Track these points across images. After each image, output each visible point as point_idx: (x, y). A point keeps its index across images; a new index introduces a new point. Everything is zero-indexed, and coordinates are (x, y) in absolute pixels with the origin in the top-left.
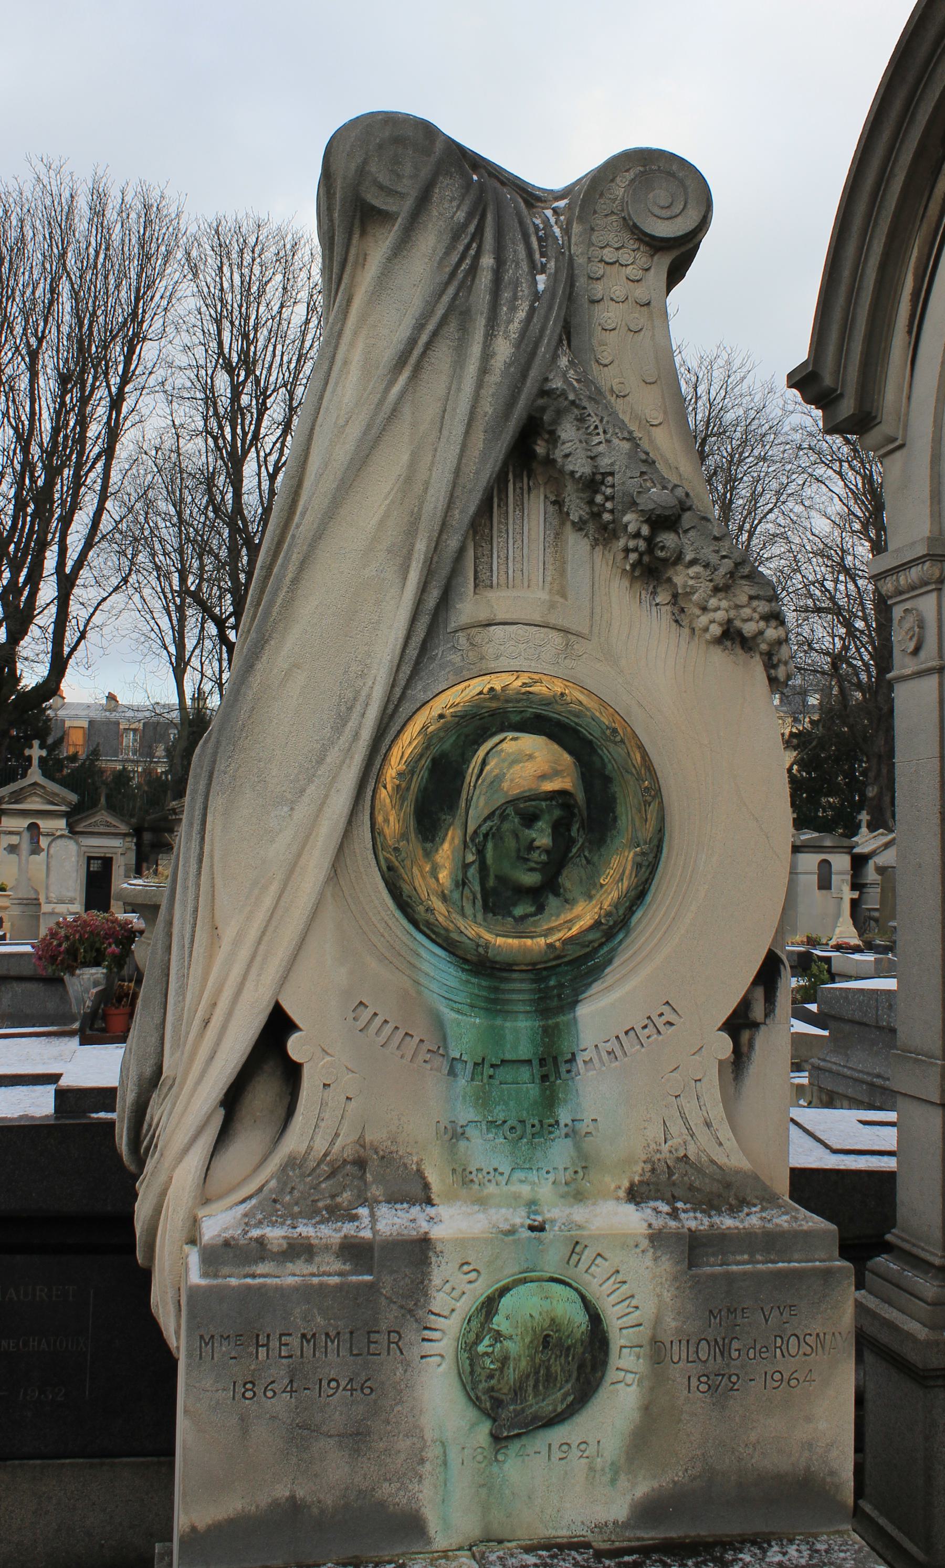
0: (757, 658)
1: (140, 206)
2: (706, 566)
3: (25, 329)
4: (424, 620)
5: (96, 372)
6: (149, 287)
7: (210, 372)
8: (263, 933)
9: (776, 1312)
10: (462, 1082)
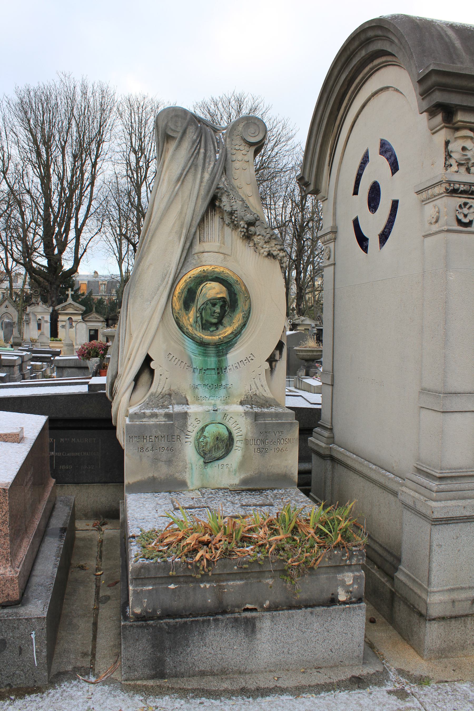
0: (278, 261)
1: (100, 91)
2: (263, 236)
3: (60, 139)
4: (185, 251)
5: (86, 154)
6: (105, 122)
7: (128, 153)
8: (144, 335)
9: (278, 433)
10: (197, 374)
